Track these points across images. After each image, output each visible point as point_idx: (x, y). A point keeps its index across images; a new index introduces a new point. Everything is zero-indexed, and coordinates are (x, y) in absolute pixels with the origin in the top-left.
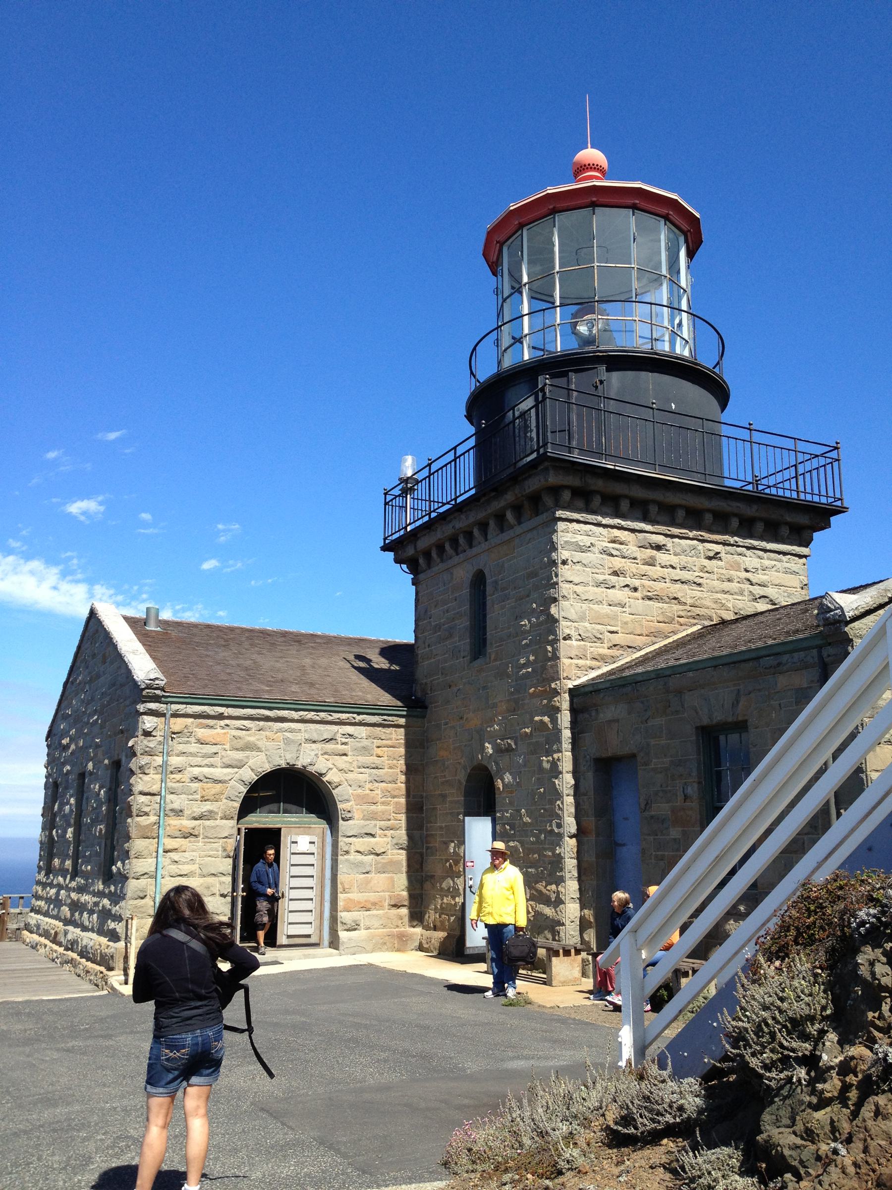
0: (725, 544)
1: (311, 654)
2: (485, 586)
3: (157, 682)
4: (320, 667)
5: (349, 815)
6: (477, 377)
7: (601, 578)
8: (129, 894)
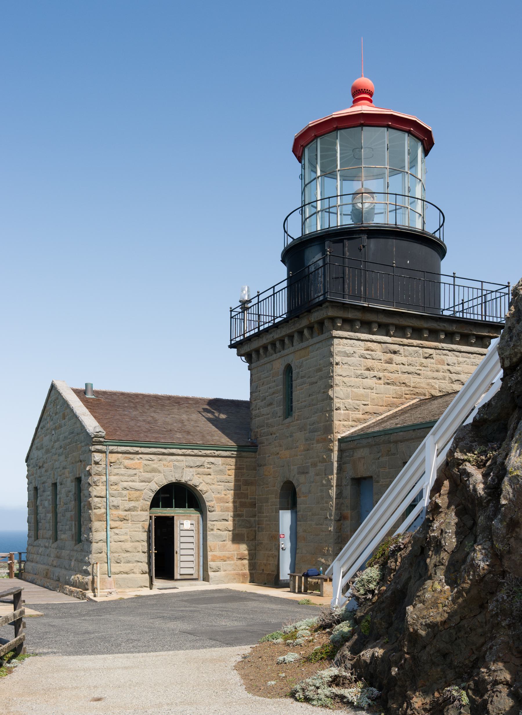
0: (436, 348)
1: (186, 412)
2: (292, 374)
3: (100, 433)
4: (193, 420)
5: (213, 509)
6: (288, 233)
7: (359, 372)
8: (93, 551)
